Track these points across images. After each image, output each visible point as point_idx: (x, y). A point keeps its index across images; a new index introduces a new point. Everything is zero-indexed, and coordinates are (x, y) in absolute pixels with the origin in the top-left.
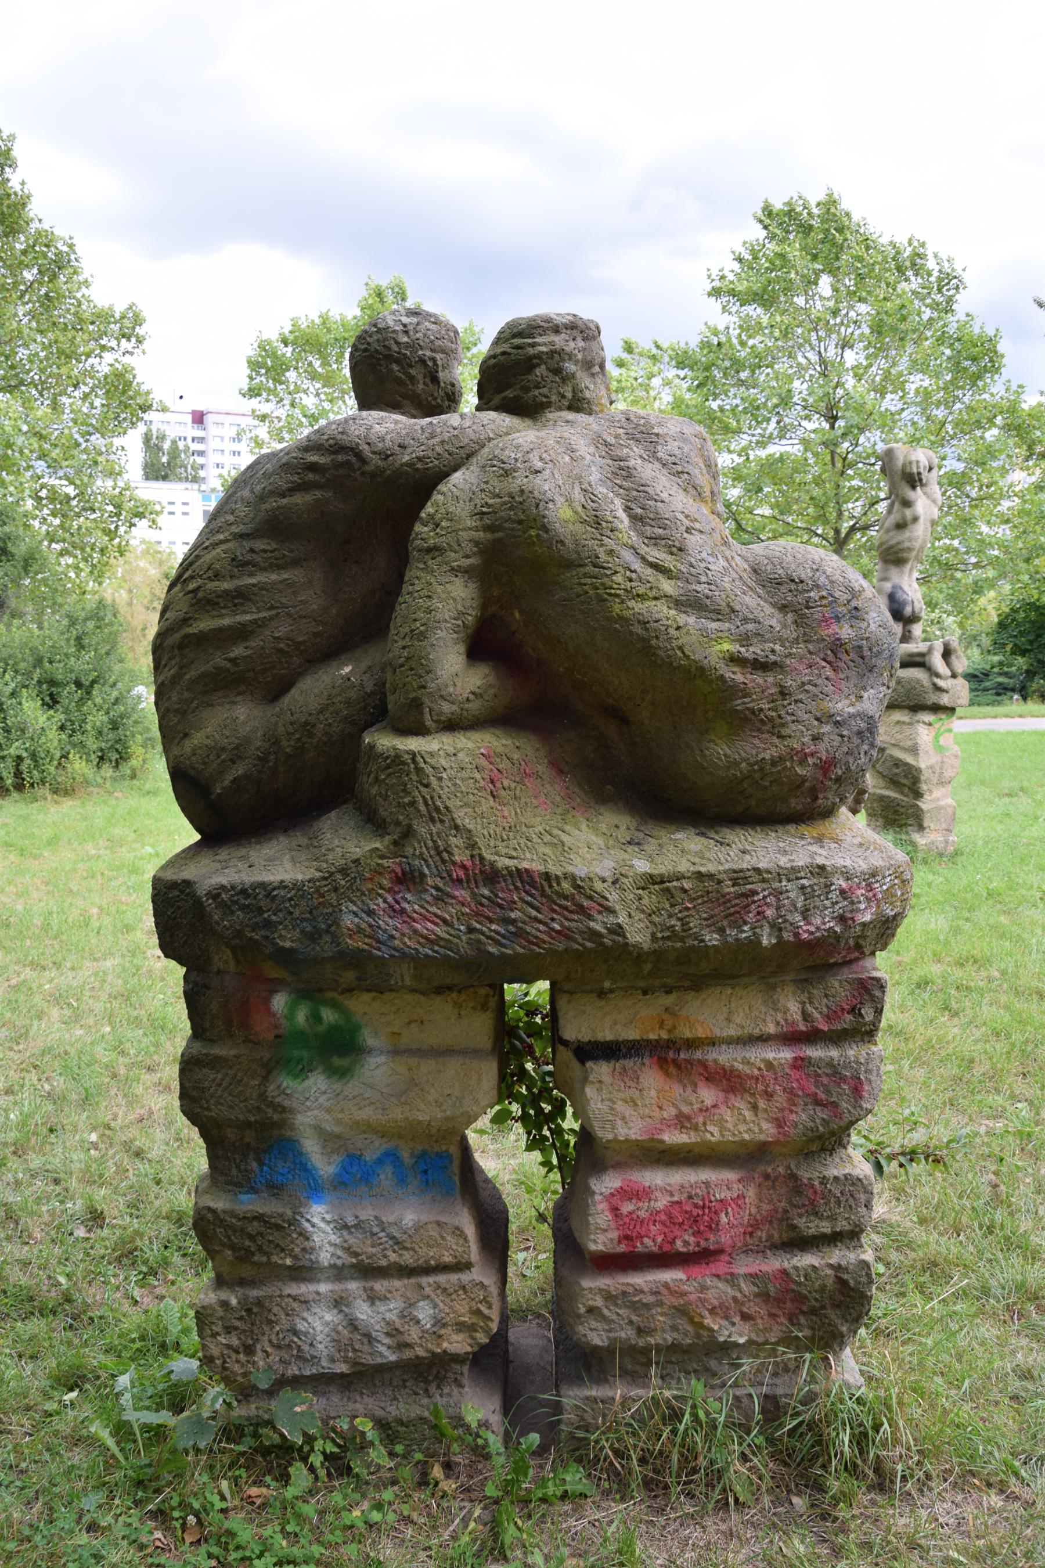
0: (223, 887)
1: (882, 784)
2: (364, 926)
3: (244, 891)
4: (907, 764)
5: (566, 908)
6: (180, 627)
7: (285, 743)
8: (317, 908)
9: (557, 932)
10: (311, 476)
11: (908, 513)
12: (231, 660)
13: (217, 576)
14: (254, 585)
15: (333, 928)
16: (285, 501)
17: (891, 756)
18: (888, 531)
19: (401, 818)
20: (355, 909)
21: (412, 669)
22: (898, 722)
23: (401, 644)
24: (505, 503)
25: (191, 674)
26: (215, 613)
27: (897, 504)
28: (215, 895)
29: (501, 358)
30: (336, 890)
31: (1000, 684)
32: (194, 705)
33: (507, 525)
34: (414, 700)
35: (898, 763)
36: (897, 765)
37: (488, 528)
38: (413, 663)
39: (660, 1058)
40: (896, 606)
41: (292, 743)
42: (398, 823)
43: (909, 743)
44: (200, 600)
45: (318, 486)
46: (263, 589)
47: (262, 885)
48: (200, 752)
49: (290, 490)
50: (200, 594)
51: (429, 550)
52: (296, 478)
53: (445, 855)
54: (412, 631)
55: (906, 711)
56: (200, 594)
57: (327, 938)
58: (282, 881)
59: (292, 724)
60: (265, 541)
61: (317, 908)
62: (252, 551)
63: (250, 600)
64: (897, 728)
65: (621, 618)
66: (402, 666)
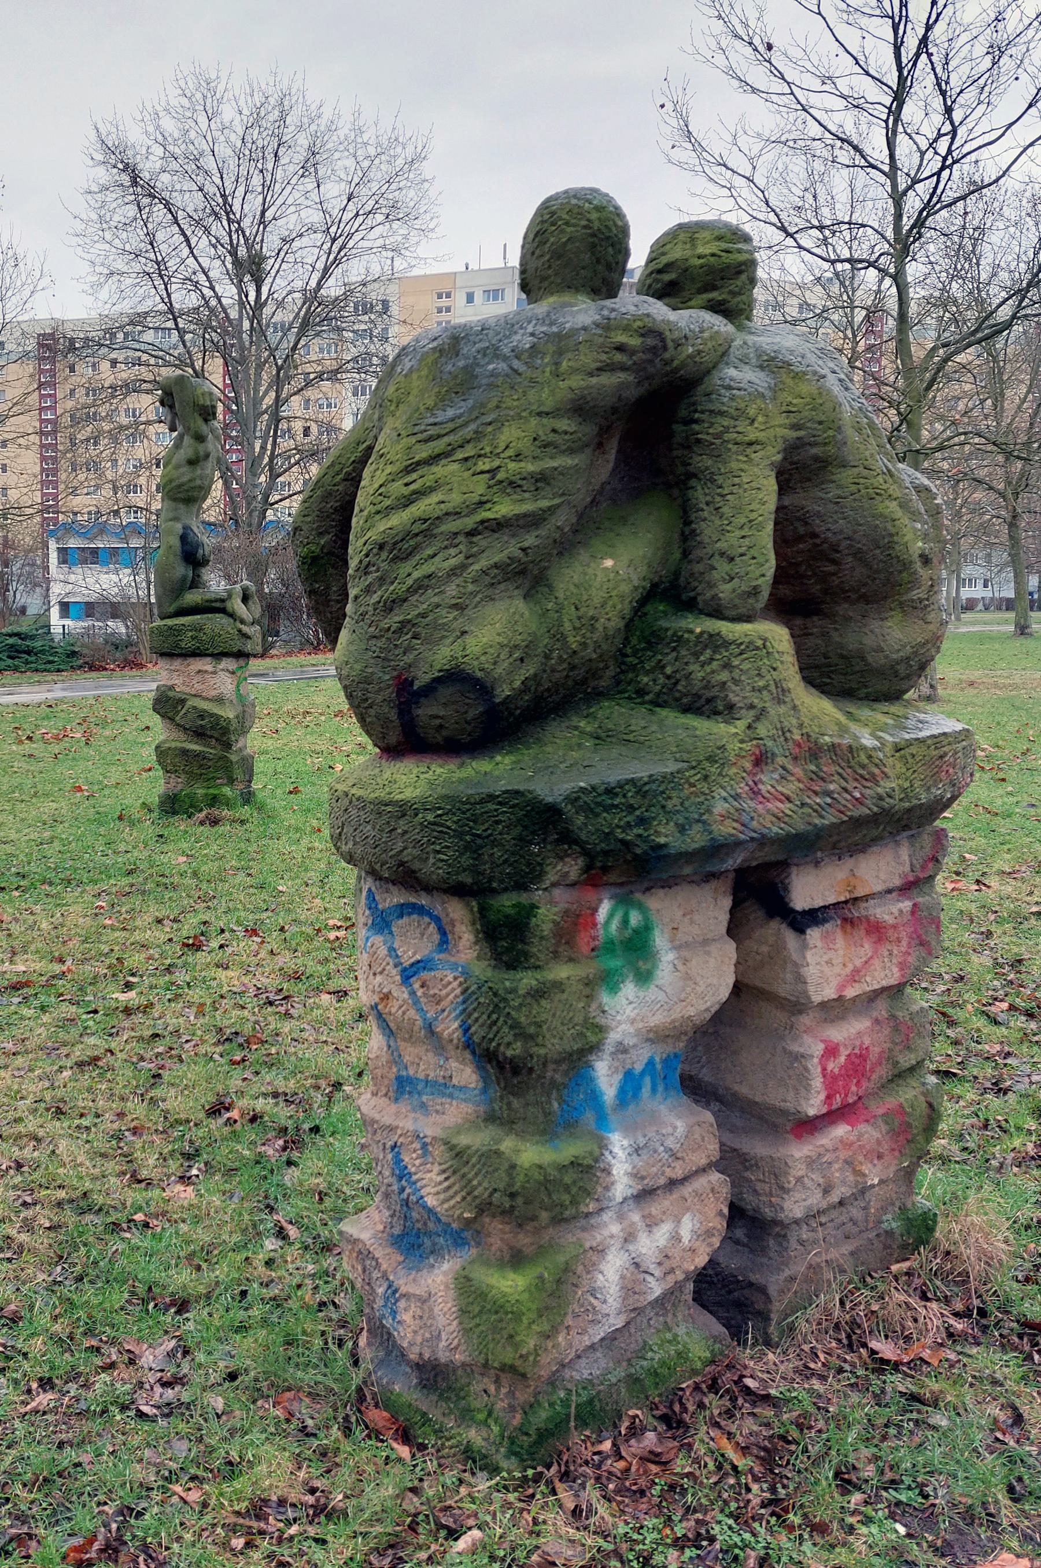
0: (582, 790)
1: (182, 736)
2: (732, 811)
3: (609, 791)
4: (212, 715)
5: (862, 776)
6: (473, 512)
7: (571, 639)
8: (688, 798)
9: (857, 799)
10: (619, 357)
11: (201, 449)
12: (523, 550)
13: (518, 457)
14: (556, 469)
15: (704, 817)
16: (594, 380)
17: (195, 708)
18: (177, 467)
19: (756, 701)
20: (724, 794)
21: (754, 558)
22: (199, 671)
23: (739, 533)
24: (808, 404)
25: (483, 563)
26: (515, 497)
27: (187, 439)
28: (573, 799)
29: (712, 259)
30: (706, 778)
31: (12, 646)
32: (477, 599)
33: (809, 425)
34: (755, 588)
35: (202, 715)
36: (202, 717)
37: (796, 427)
38: (753, 552)
39: (845, 920)
40: (188, 548)
41: (578, 638)
42: (752, 707)
43: (214, 693)
44: (501, 482)
45: (623, 368)
46: (561, 474)
47: (632, 781)
48: (491, 651)
49: (599, 369)
50: (501, 476)
51: (750, 444)
52: (604, 357)
53: (788, 735)
54: (750, 521)
55: (209, 659)
56: (501, 476)
57: (698, 827)
58: (651, 776)
59: (579, 618)
60: (566, 422)
61: (688, 798)
62: (554, 431)
63: (548, 484)
64: (199, 678)
65: (882, 515)
66: (742, 555)
